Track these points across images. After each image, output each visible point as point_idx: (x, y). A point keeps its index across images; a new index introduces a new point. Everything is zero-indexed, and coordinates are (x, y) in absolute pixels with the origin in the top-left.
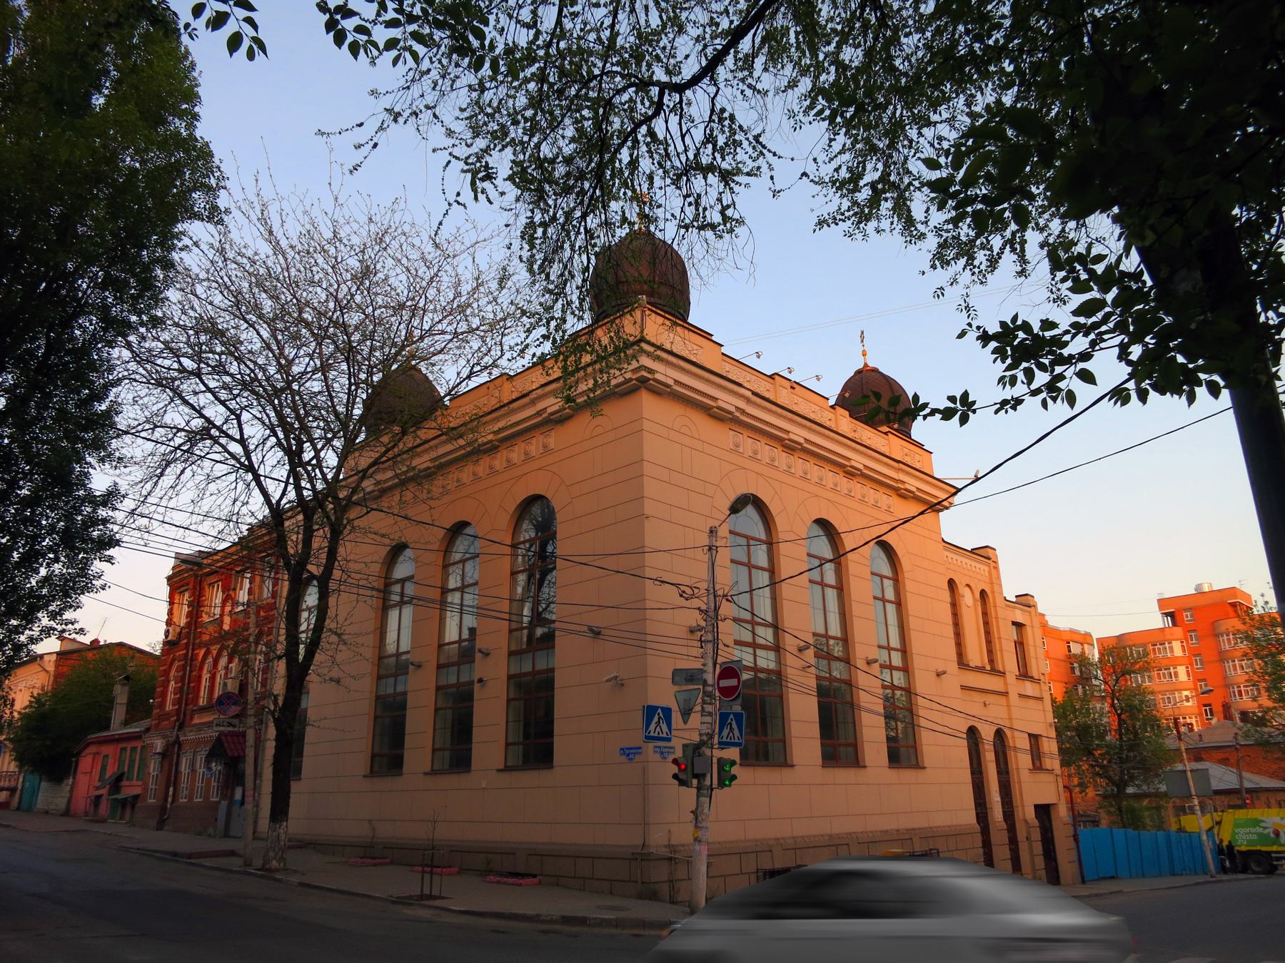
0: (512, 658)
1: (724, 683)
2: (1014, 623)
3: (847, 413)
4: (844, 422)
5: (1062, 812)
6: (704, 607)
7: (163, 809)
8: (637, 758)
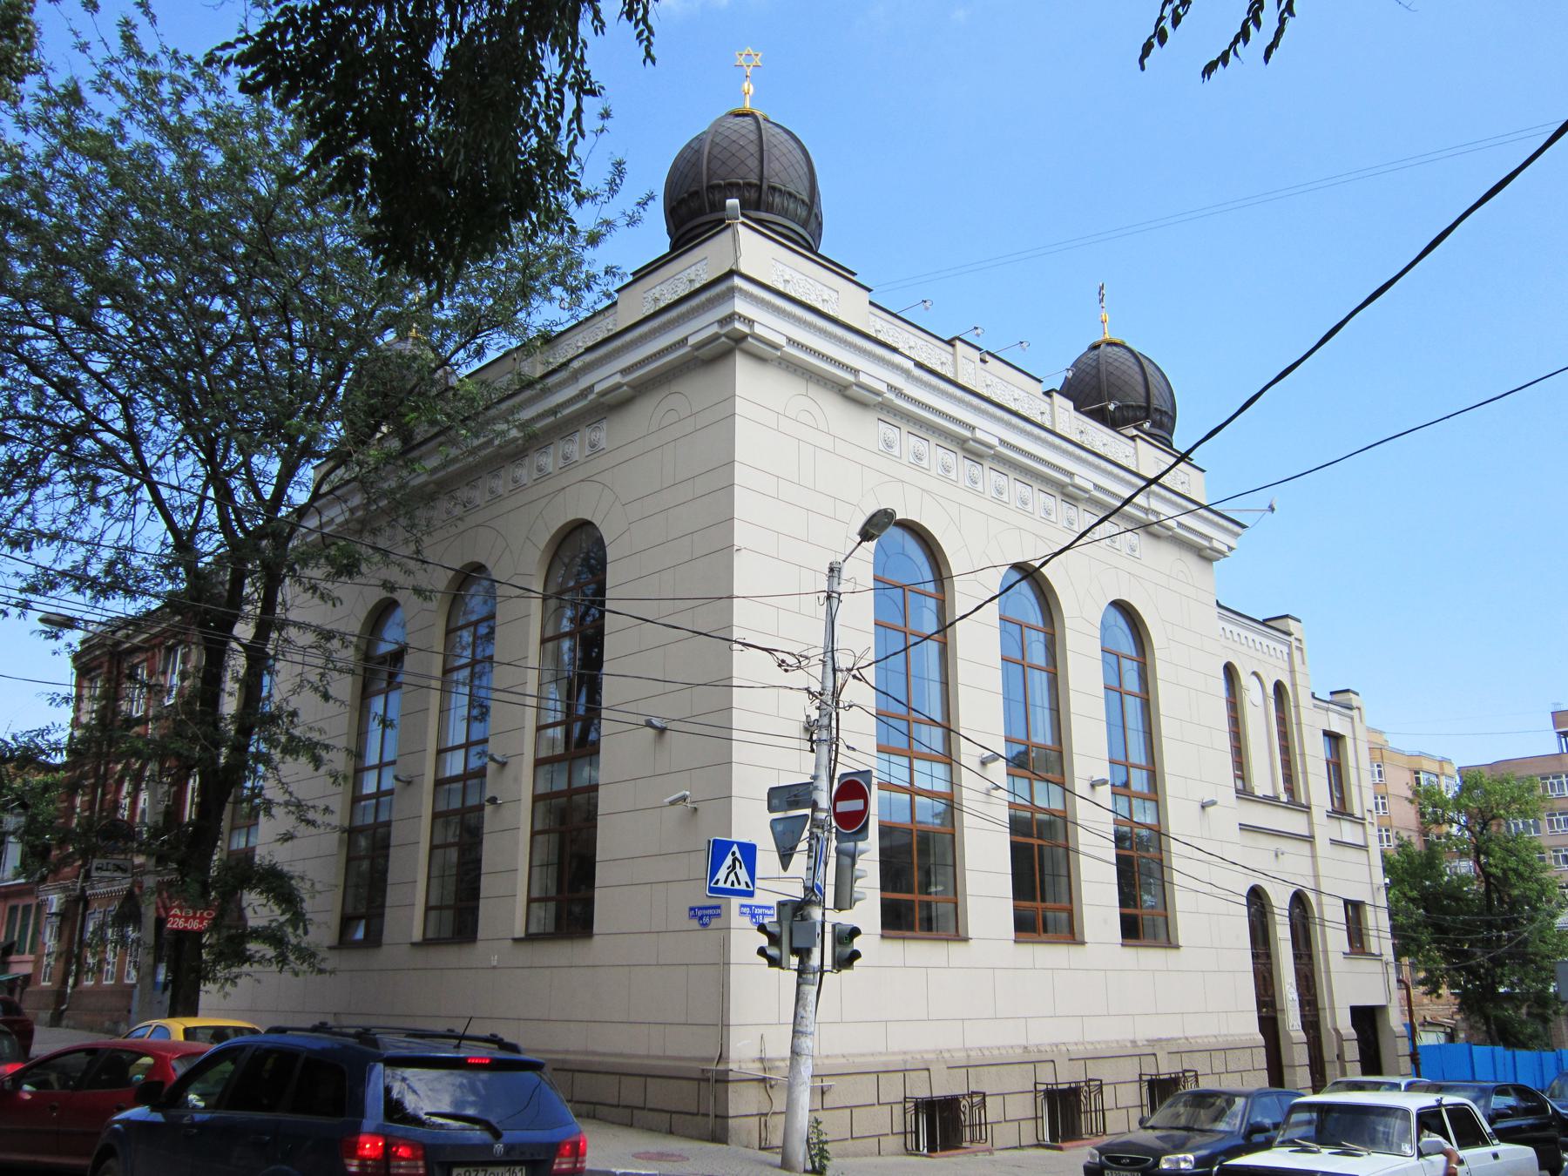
0: (544, 769)
1: (843, 806)
2: (1327, 734)
3: (1070, 405)
4: (1066, 418)
6: (816, 688)
7: (60, 996)
8: (715, 923)
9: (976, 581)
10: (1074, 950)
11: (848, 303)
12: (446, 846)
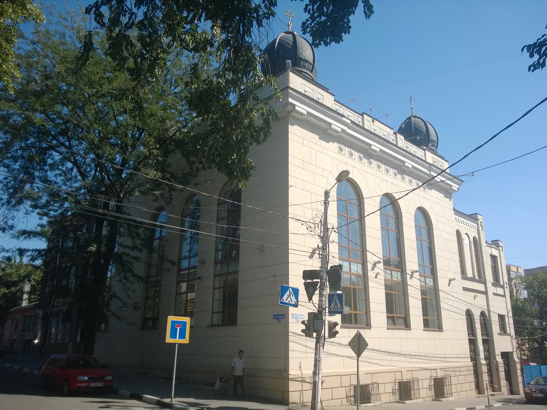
4: (401, 141)
9: (372, 205)
10: (407, 332)
11: (328, 100)
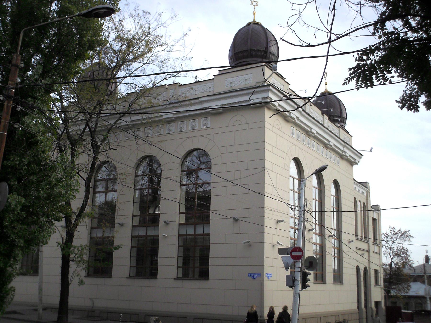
5: (383, 305)
8: (258, 278)
12: (134, 247)
